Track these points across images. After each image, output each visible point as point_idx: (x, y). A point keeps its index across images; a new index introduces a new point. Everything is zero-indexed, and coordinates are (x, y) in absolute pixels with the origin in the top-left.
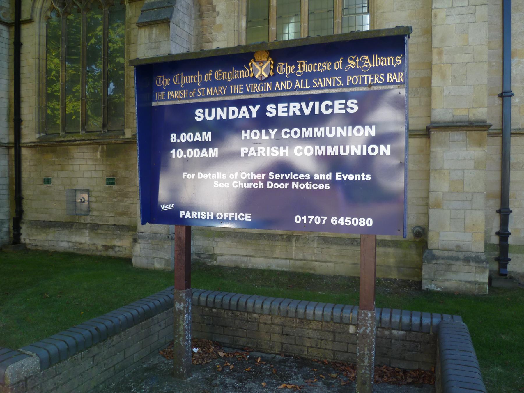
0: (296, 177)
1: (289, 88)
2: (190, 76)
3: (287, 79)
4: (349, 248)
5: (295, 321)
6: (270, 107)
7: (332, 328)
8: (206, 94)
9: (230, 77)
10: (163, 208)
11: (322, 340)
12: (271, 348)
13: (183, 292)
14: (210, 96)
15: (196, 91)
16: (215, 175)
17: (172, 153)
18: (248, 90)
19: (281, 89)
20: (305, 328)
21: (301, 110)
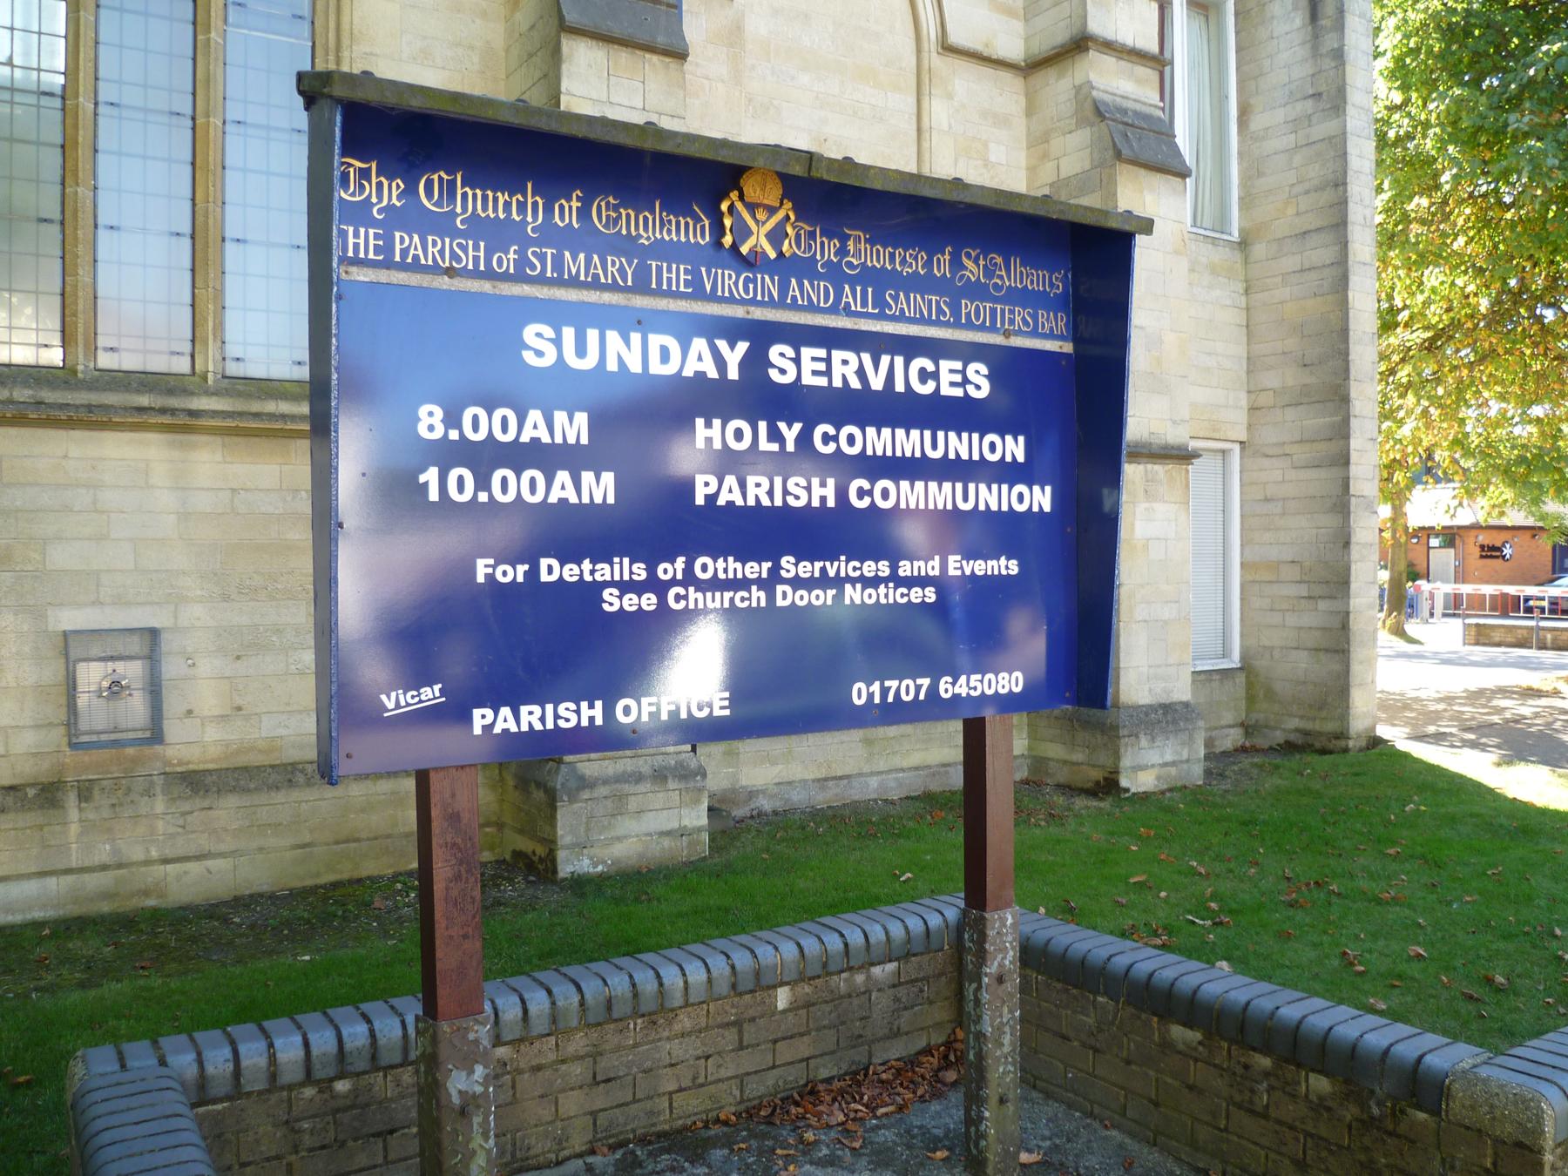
0: (855, 569)
1: (826, 302)
2: (495, 191)
3: (821, 277)
4: (279, 797)
5: (632, 1026)
6: (778, 353)
7: (734, 1011)
8: (561, 273)
9: (646, 229)
10: (390, 705)
11: (707, 1057)
12: (560, 1143)
13: (482, 1024)
14: (574, 282)
15: (522, 253)
16: (607, 567)
17: (426, 483)
18: (708, 288)
19: (589, 279)
20: (660, 1040)
21: (861, 373)
